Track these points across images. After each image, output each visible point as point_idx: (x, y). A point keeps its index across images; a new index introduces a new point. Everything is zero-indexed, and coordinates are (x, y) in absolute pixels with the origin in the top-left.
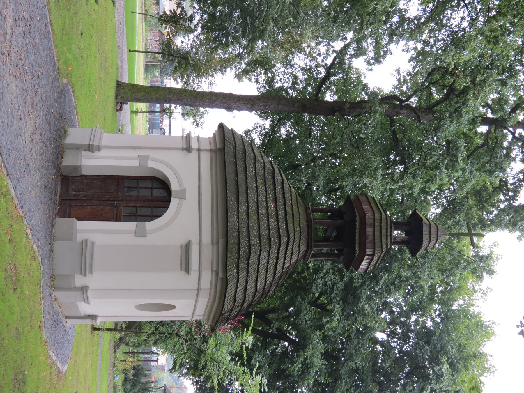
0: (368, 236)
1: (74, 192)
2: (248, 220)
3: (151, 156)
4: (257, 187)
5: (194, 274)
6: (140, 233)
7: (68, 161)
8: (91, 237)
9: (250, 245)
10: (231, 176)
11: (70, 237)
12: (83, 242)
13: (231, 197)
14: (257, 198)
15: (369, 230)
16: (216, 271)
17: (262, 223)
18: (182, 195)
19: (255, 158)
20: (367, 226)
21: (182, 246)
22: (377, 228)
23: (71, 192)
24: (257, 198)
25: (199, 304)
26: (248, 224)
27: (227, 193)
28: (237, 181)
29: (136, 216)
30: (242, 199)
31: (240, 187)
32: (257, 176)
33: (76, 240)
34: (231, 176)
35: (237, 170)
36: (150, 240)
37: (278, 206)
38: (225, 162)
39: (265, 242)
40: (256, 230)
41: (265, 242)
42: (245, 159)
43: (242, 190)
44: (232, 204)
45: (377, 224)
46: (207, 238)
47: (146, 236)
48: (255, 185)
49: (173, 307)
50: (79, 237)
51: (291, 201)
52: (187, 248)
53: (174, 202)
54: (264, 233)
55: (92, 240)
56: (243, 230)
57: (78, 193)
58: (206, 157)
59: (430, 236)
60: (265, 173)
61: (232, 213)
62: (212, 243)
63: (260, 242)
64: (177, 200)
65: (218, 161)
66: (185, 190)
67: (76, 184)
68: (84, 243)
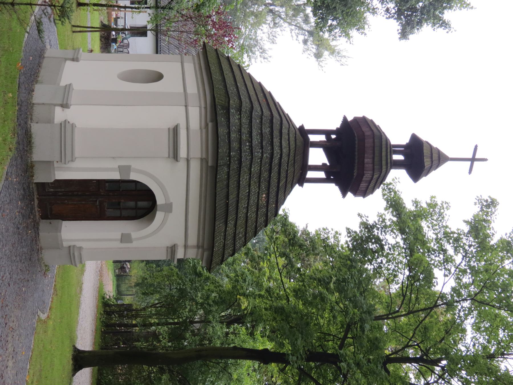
1: (52, 190)
3: (133, 166)
4: (249, 192)
5: (182, 165)
7: (40, 177)
8: (78, 244)
11: (57, 245)
12: (61, 124)
14: (248, 202)
18: (168, 208)
19: (252, 107)
21: (169, 129)
23: (48, 190)
24: (248, 202)
25: (186, 65)
29: (120, 209)
33: (53, 122)
35: (228, 192)
38: (215, 207)
46: (193, 240)
47: (132, 243)
49: (159, 77)
57: (57, 190)
58: (195, 167)
60: (261, 168)
62: (201, 128)
65: (209, 178)
66: (171, 204)
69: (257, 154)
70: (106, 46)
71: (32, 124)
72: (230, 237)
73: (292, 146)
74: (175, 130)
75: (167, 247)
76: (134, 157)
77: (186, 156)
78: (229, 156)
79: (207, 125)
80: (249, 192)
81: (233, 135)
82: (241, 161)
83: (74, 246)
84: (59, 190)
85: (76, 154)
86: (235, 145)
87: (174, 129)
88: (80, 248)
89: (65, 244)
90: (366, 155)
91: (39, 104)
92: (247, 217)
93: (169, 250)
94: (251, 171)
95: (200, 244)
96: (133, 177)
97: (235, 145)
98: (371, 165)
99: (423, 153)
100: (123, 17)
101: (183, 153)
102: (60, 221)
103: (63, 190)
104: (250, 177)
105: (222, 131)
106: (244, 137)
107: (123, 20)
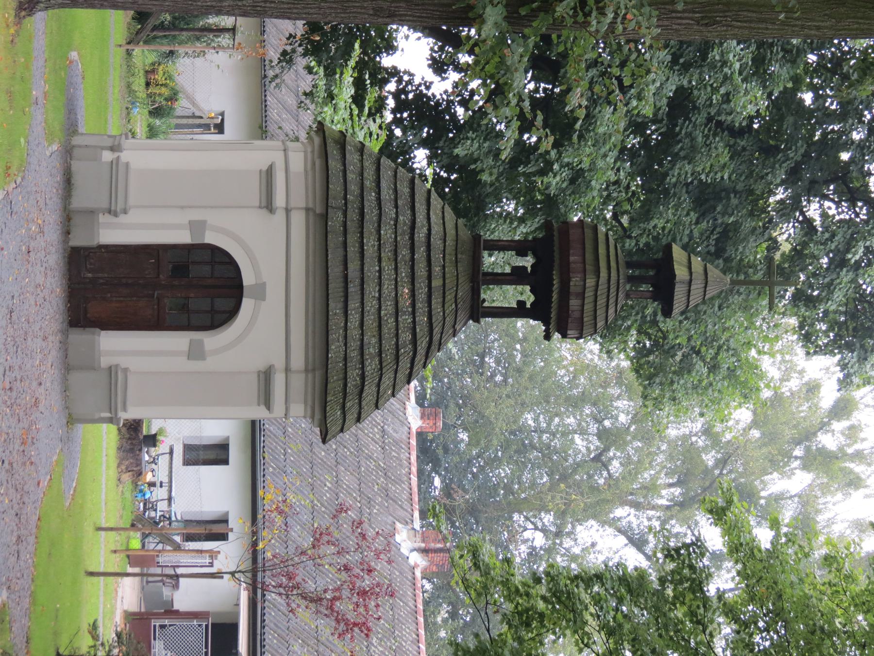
0: (573, 311)
1: (90, 275)
2: (362, 334)
3: (209, 222)
4: (380, 271)
5: (280, 217)
6: (196, 353)
8: (124, 362)
9: (363, 374)
10: (335, 271)
13: (335, 307)
14: (380, 291)
15: (574, 303)
16: (321, 215)
17: (385, 330)
18: (260, 292)
20: (571, 297)
21: (261, 171)
22: (589, 299)
24: (380, 291)
26: (362, 340)
27: (328, 305)
28: (346, 277)
30: (354, 304)
31: (351, 285)
32: (382, 250)
34: (335, 271)
35: (346, 256)
36: (210, 364)
37: (417, 285)
39: (388, 358)
40: (374, 347)
41: (388, 358)
42: (362, 228)
43: (353, 289)
44: (336, 320)
45: (589, 293)
46: (298, 360)
48: (377, 268)
50: (105, 362)
51: (444, 260)
52: (266, 377)
53: (247, 304)
54: (388, 345)
55: (123, 366)
56: (354, 354)
58: (299, 220)
59: (688, 299)
60: (396, 237)
61: (336, 335)
63: (381, 363)
64: (252, 301)
66: (264, 284)
67: (92, 261)
68: (111, 371)
69: (389, 210)
70: (132, 443)
71: (72, 162)
72: (354, 344)
73: (450, 242)
74: (269, 174)
75: (259, 372)
76: (212, 207)
77: (284, 205)
78: (345, 198)
79: (314, 164)
80: (380, 271)
81: (351, 176)
82: (363, 212)
83: (117, 366)
84: (100, 275)
85: (132, 201)
86: (353, 188)
87: (267, 170)
88: (126, 370)
89: (105, 362)
90: (571, 251)
91: (80, 146)
92: (380, 318)
93: (262, 376)
94: (380, 235)
95: (310, 367)
96: (210, 239)
97: (353, 188)
98: (580, 266)
99: (672, 258)
100: (165, 480)
101: (280, 200)
102: (98, 330)
103: (106, 275)
104: (380, 245)
105: (335, 164)
106: (367, 183)
107: (165, 489)
